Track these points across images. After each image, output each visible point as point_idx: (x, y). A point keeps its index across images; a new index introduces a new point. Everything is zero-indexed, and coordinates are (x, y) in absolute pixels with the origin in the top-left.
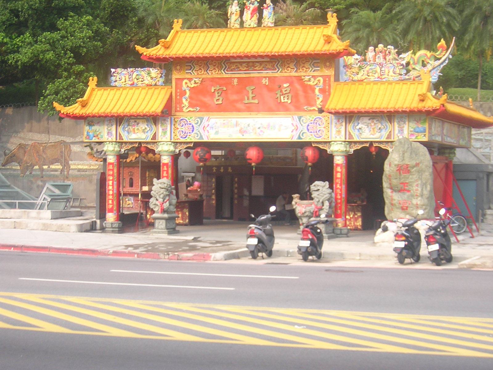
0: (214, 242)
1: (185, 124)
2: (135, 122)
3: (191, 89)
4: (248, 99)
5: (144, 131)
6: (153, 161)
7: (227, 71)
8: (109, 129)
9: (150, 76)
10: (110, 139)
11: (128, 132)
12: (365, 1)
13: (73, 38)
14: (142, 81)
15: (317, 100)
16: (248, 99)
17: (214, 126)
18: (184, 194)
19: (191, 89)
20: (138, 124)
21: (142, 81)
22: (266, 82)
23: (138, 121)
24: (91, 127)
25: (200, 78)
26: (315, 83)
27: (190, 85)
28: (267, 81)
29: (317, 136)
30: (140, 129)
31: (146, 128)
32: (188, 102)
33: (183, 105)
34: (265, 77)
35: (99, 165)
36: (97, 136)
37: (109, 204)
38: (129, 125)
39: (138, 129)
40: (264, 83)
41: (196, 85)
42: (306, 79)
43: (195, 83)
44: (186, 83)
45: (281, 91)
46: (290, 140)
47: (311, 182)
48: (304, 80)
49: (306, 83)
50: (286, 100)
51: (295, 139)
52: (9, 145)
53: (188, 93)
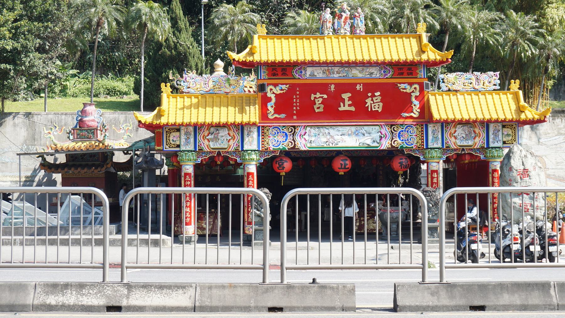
0: (357, 311)
1: (278, 133)
3: (277, 96)
4: (344, 106)
9: (228, 82)
12: (3, 172)
13: (158, 157)
14: (219, 88)
15: (414, 107)
16: (344, 106)
19: (277, 96)
21: (219, 88)
22: (360, 88)
26: (411, 91)
27: (275, 92)
28: (361, 87)
29: (277, 129)
32: (273, 108)
33: (268, 112)
34: (360, 84)
37: (186, 218)
40: (358, 89)
41: (282, 92)
42: (401, 87)
43: (282, 90)
44: (271, 90)
45: (372, 100)
48: (400, 88)
49: (402, 90)
50: (376, 109)
53: (274, 100)
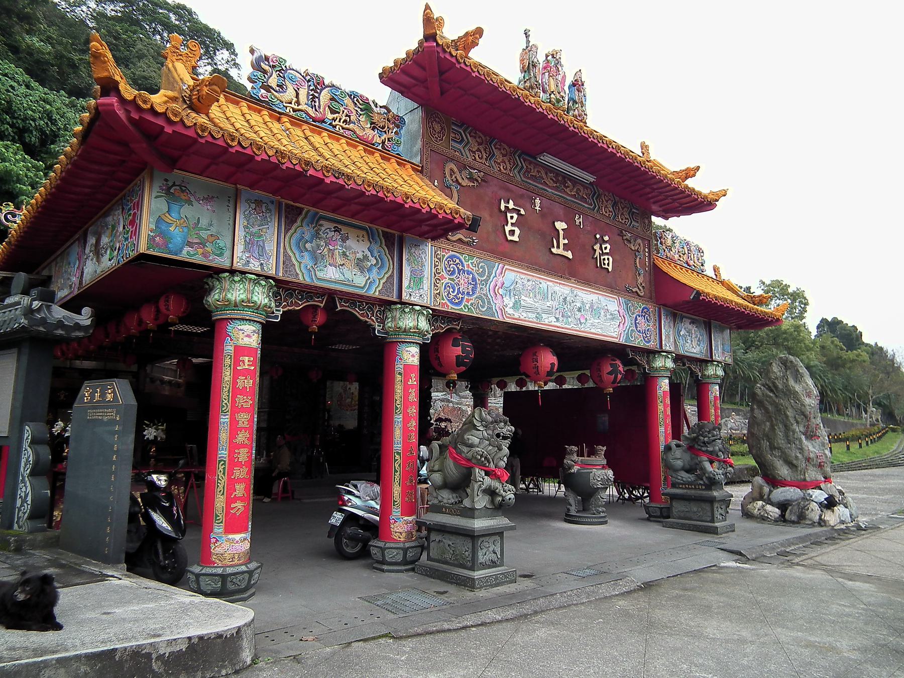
2: (337, 230)
5: (360, 264)
6: (688, 466)
7: (525, 176)
8: (255, 230)
10: (255, 266)
11: (316, 258)
17: (512, 288)
18: (98, 260)
20: (344, 239)
23: (344, 230)
24: (175, 207)
25: (480, 171)
30: (351, 257)
31: (366, 258)
35: (216, 315)
36: (202, 244)
38: (317, 235)
39: (344, 254)
46: (616, 341)
47: (808, 482)
51: (622, 341)
52: (345, 497)
